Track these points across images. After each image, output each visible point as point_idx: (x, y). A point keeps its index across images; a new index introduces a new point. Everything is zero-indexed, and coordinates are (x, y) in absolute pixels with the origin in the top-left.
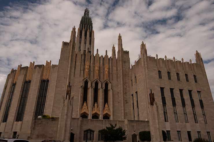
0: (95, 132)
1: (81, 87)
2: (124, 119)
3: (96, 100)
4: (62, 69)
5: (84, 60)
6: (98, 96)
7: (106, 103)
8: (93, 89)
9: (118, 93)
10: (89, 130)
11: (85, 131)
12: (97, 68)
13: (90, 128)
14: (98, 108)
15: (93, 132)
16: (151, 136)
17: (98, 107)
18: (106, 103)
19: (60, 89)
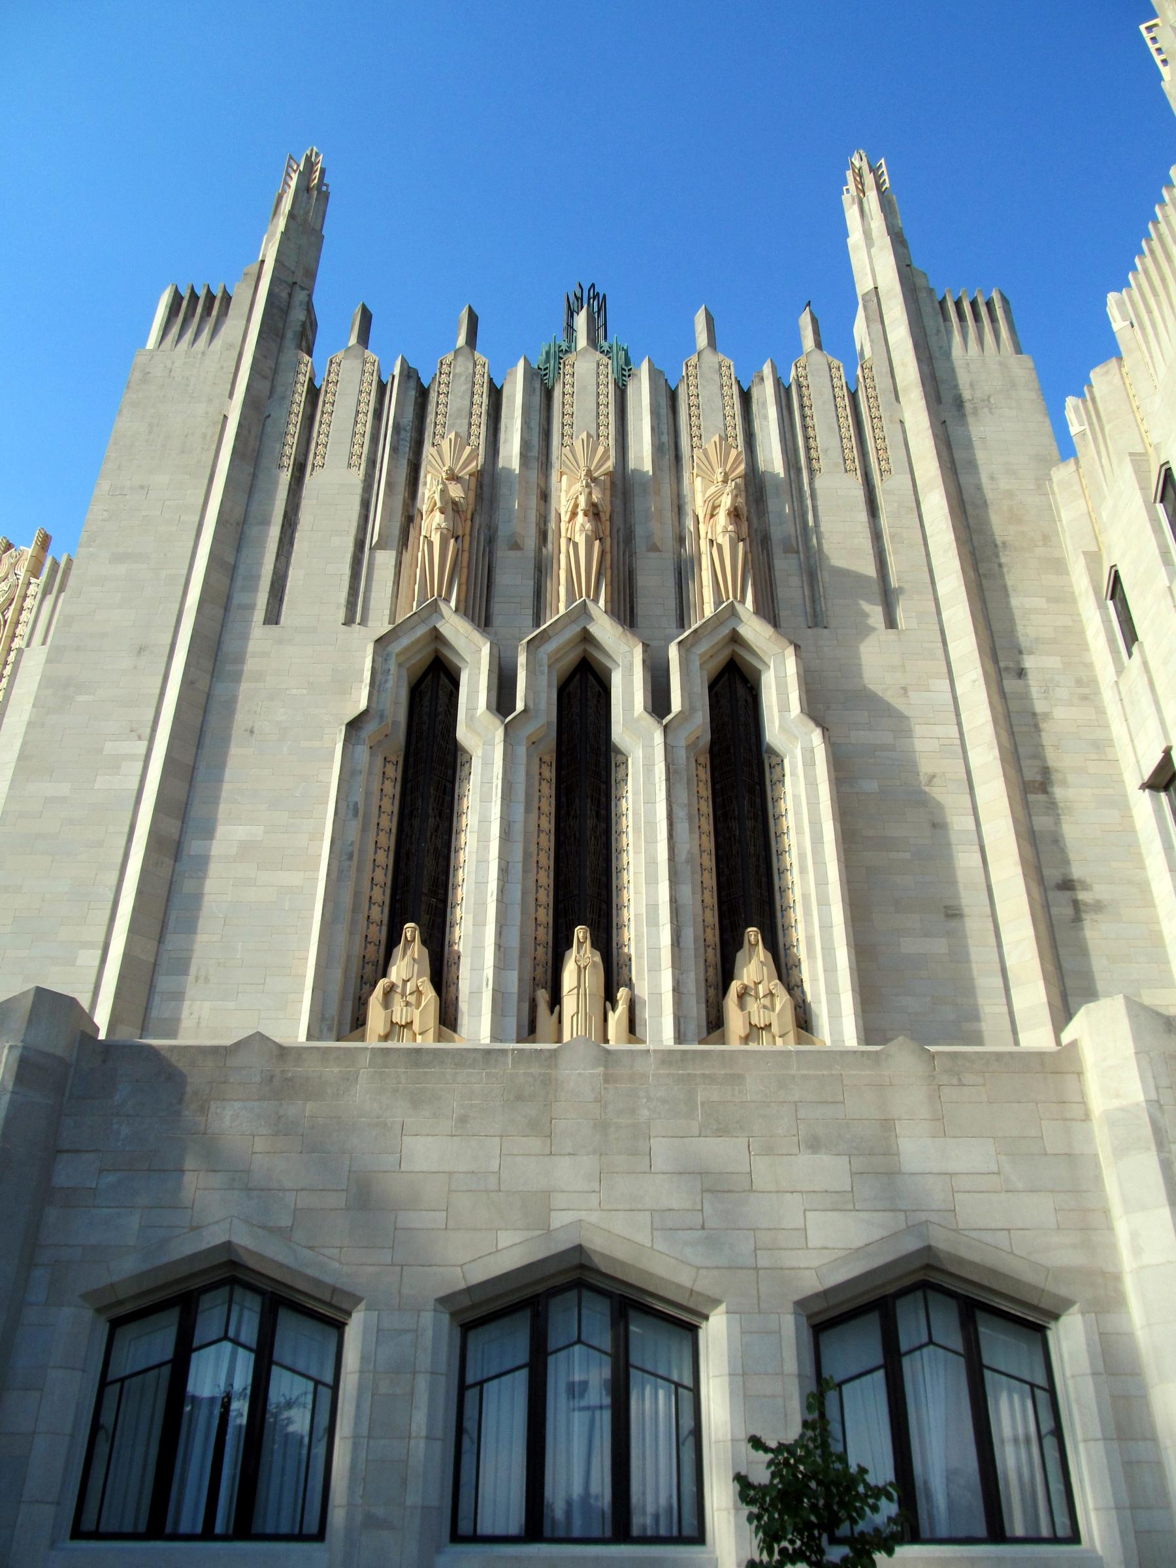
0: (716, 1331)
1: (354, 726)
2: (1063, 1010)
3: (577, 887)
4: (117, 559)
5: (407, 436)
6: (550, 773)
7: (752, 933)
8: (522, 751)
9: (905, 689)
10: (230, 1274)
11: (123, 1318)
12: (569, 493)
13: (244, 1239)
14: (617, 1018)
15: (684, 1327)
16: (608, 1313)
17: (610, 997)
18: (752, 933)
19: (64, 789)
